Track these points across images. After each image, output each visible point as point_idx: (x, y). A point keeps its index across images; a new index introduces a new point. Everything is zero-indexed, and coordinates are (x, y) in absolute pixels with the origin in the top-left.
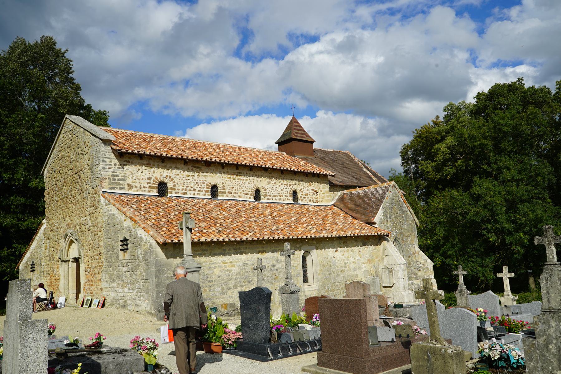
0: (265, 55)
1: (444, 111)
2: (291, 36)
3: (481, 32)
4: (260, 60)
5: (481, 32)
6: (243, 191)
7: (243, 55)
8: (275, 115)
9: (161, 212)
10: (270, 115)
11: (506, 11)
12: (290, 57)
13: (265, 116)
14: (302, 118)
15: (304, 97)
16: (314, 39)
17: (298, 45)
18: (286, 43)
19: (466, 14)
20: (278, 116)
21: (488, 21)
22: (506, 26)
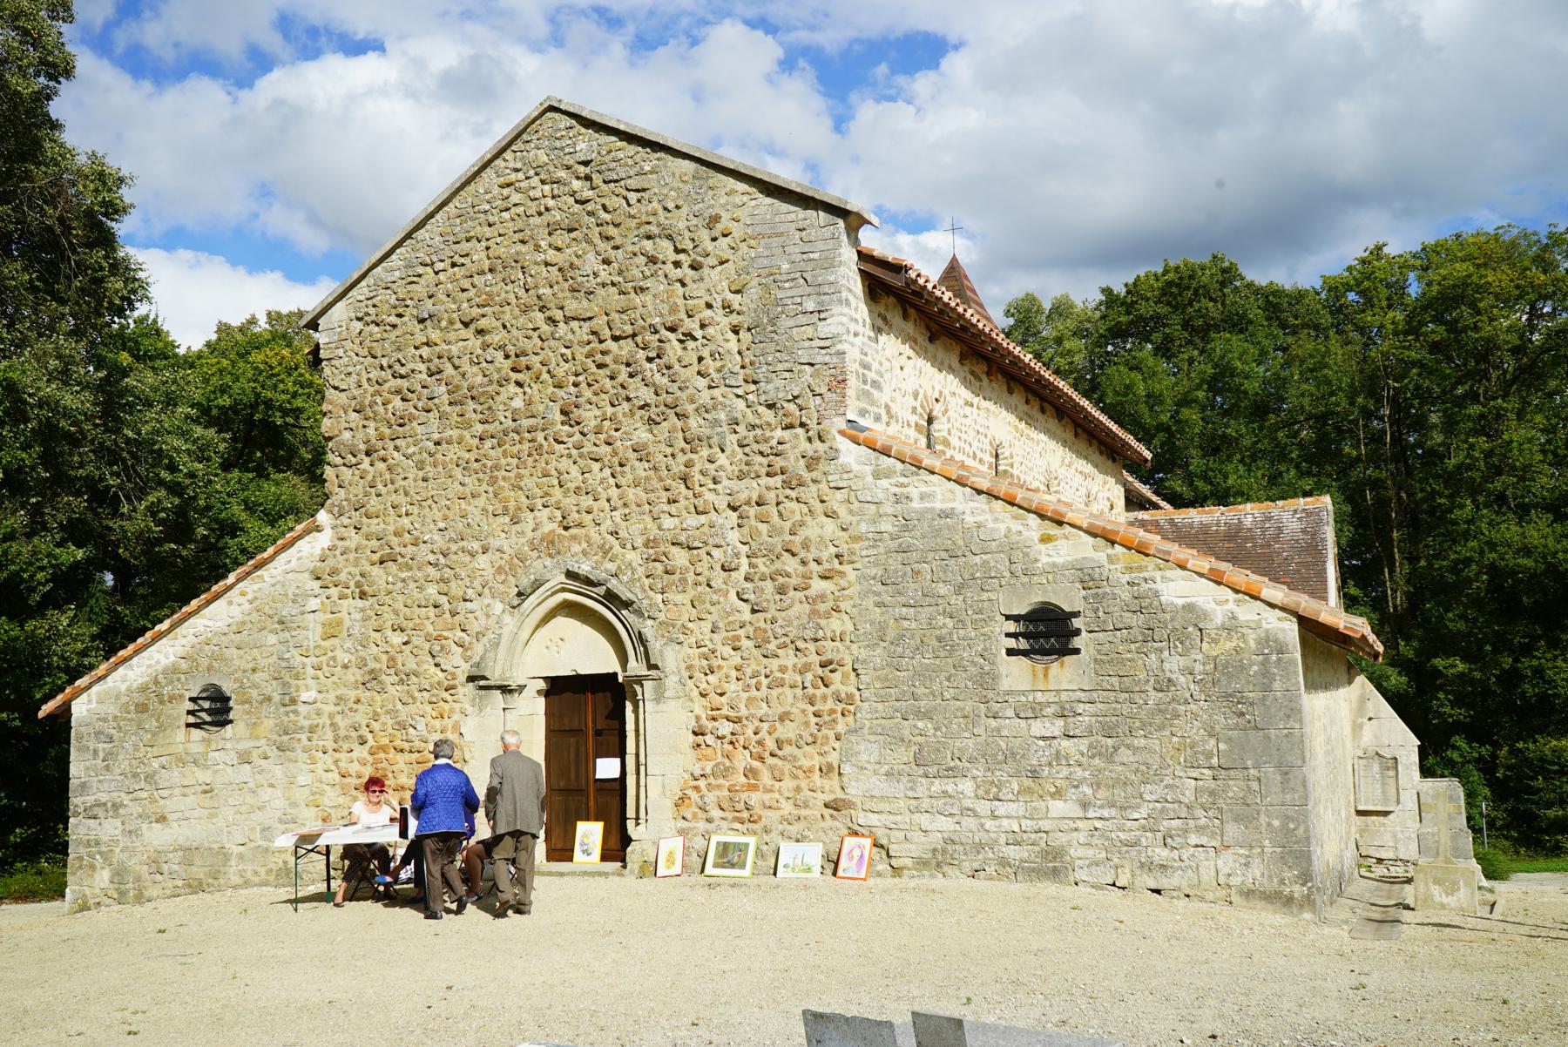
0: (201, 64)
1: (269, 314)
2: (284, 23)
3: (840, 124)
4: (654, 48)
5: (840, 124)
6: (804, 563)
7: (120, 48)
8: (222, 259)
9: (142, 584)
10: (203, 256)
11: (901, 80)
12: (278, 84)
13: (186, 255)
14: (314, 284)
15: (314, 220)
16: (355, 47)
17: (310, 52)
18: (272, 41)
19: (802, 63)
20: (234, 262)
21: (854, 97)
22: (900, 116)
